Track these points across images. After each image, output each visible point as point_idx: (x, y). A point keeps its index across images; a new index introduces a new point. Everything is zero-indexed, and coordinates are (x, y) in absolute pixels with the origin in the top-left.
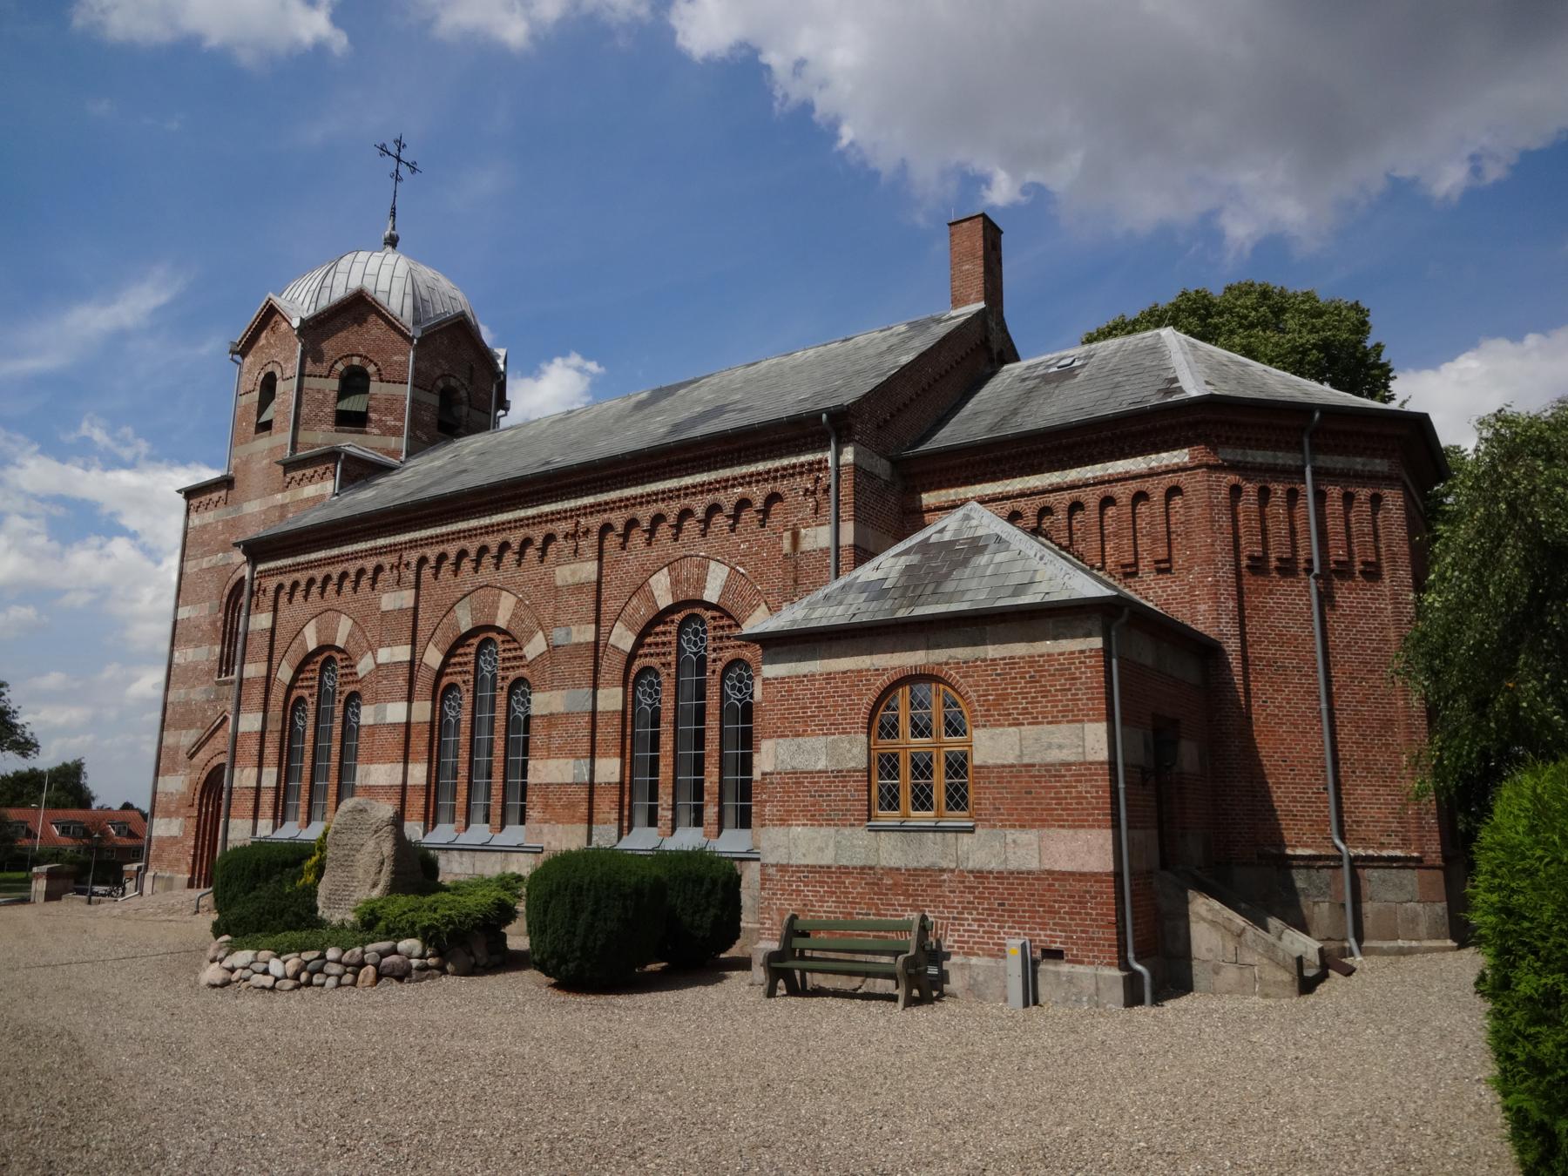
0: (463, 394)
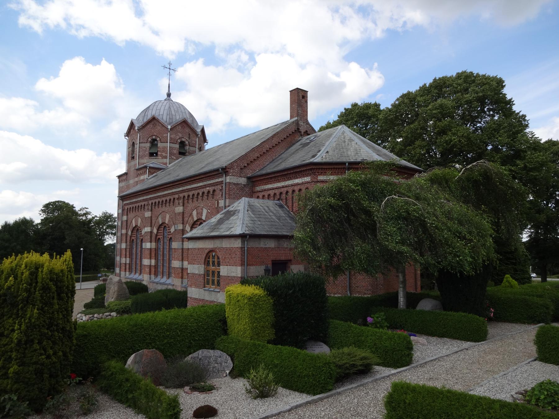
0: (187, 143)
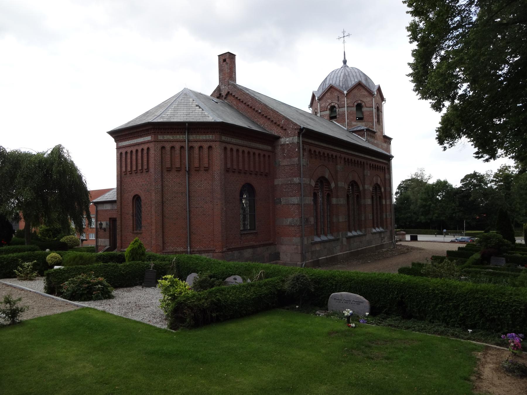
0: (336, 106)
